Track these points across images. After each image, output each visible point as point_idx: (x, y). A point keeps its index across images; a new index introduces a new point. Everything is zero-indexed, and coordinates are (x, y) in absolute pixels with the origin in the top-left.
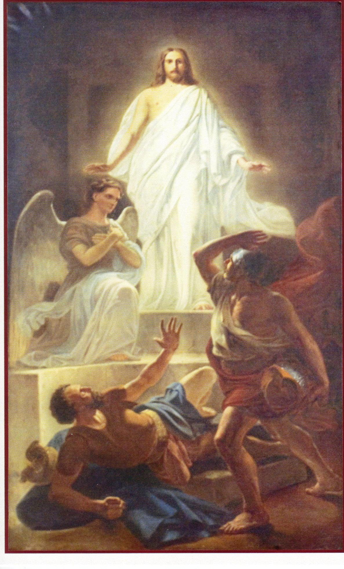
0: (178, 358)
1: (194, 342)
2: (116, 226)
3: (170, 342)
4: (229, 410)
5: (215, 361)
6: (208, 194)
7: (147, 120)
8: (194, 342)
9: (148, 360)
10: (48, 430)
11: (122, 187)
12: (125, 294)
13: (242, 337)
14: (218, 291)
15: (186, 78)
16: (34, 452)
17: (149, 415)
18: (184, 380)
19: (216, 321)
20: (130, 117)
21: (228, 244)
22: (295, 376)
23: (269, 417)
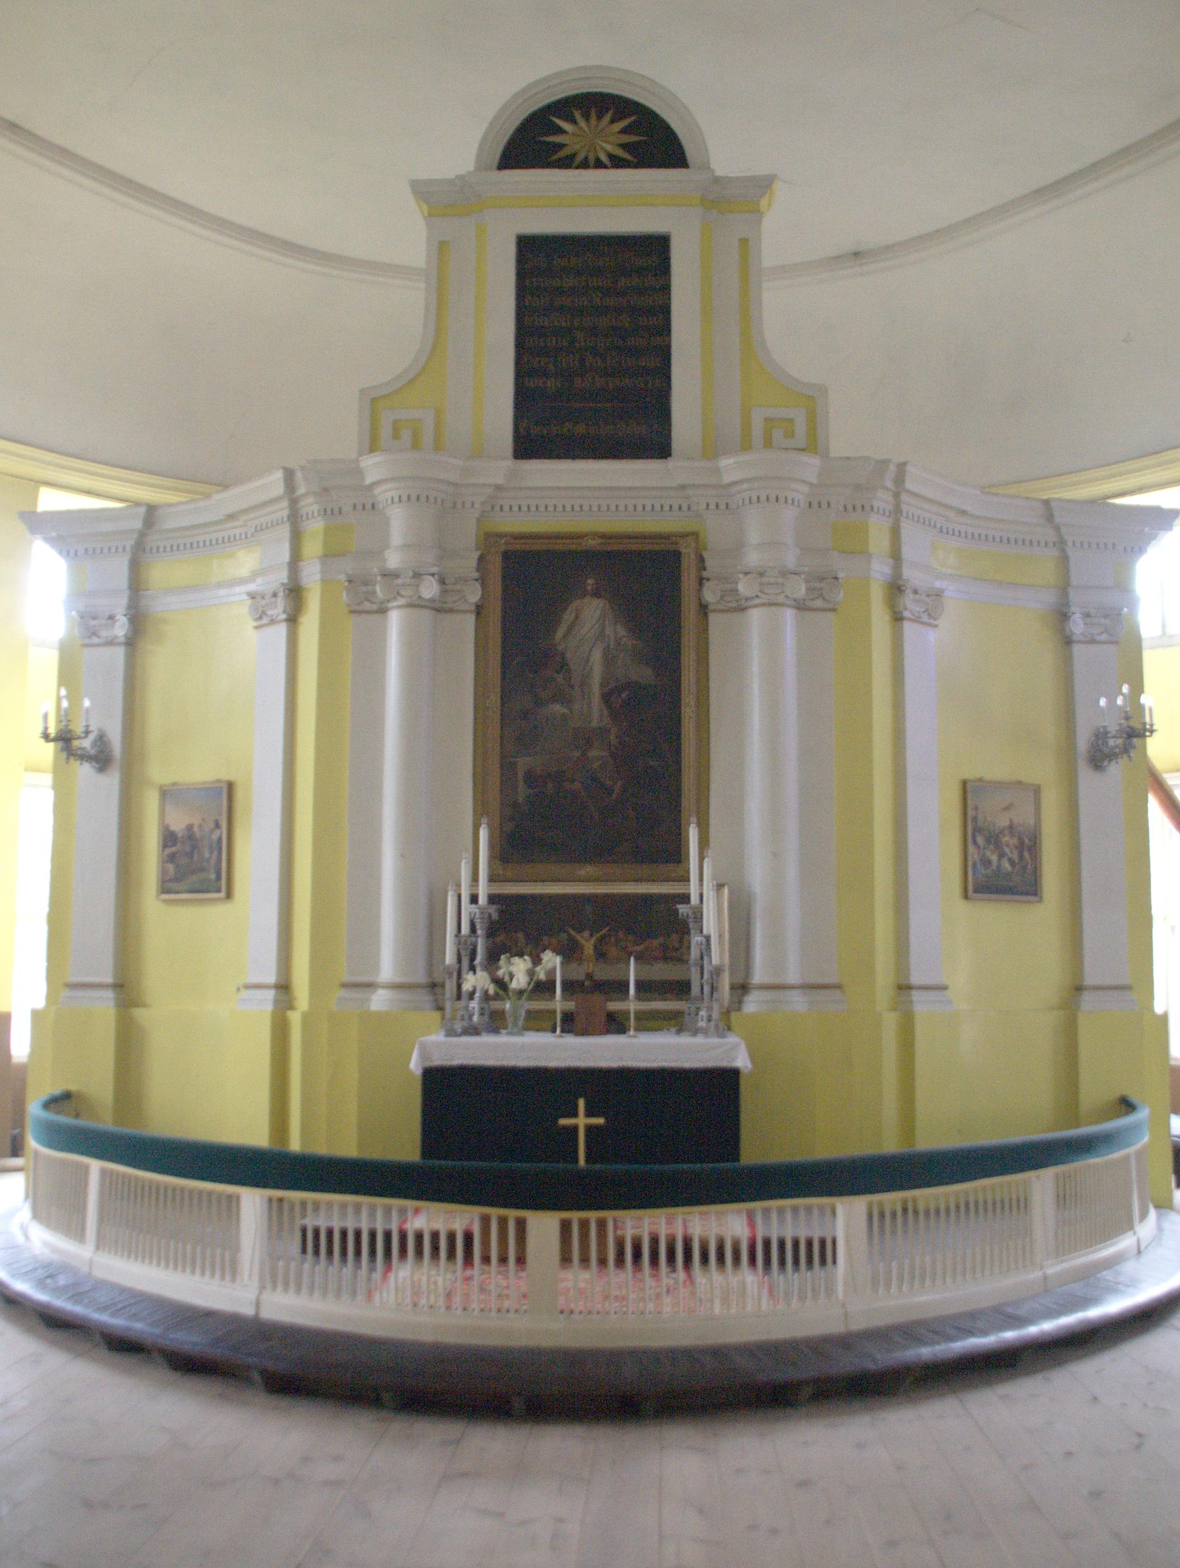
0: (593, 753)
1: (593, 342)
2: (560, 678)
3: (589, 743)
4: (619, 783)
5: (612, 755)
6: (609, 660)
7: (577, 617)
8: (593, 342)
9: (577, 754)
10: (522, 792)
11: (563, 655)
12: (564, 718)
13: (767, 195)
14: (614, 716)
15: (597, 594)
16: (515, 805)
17: (577, 786)
18: (595, 765)
19: (614, 731)
20: (568, 616)
21: (619, 690)
22: (655, 764)
23: (261, 1293)
